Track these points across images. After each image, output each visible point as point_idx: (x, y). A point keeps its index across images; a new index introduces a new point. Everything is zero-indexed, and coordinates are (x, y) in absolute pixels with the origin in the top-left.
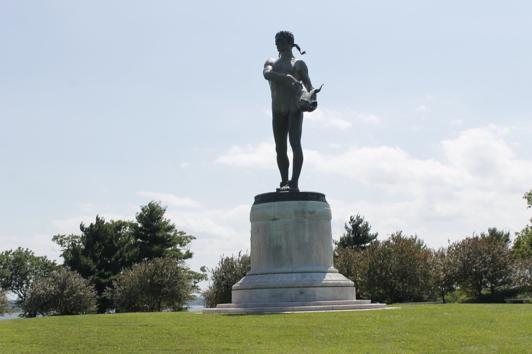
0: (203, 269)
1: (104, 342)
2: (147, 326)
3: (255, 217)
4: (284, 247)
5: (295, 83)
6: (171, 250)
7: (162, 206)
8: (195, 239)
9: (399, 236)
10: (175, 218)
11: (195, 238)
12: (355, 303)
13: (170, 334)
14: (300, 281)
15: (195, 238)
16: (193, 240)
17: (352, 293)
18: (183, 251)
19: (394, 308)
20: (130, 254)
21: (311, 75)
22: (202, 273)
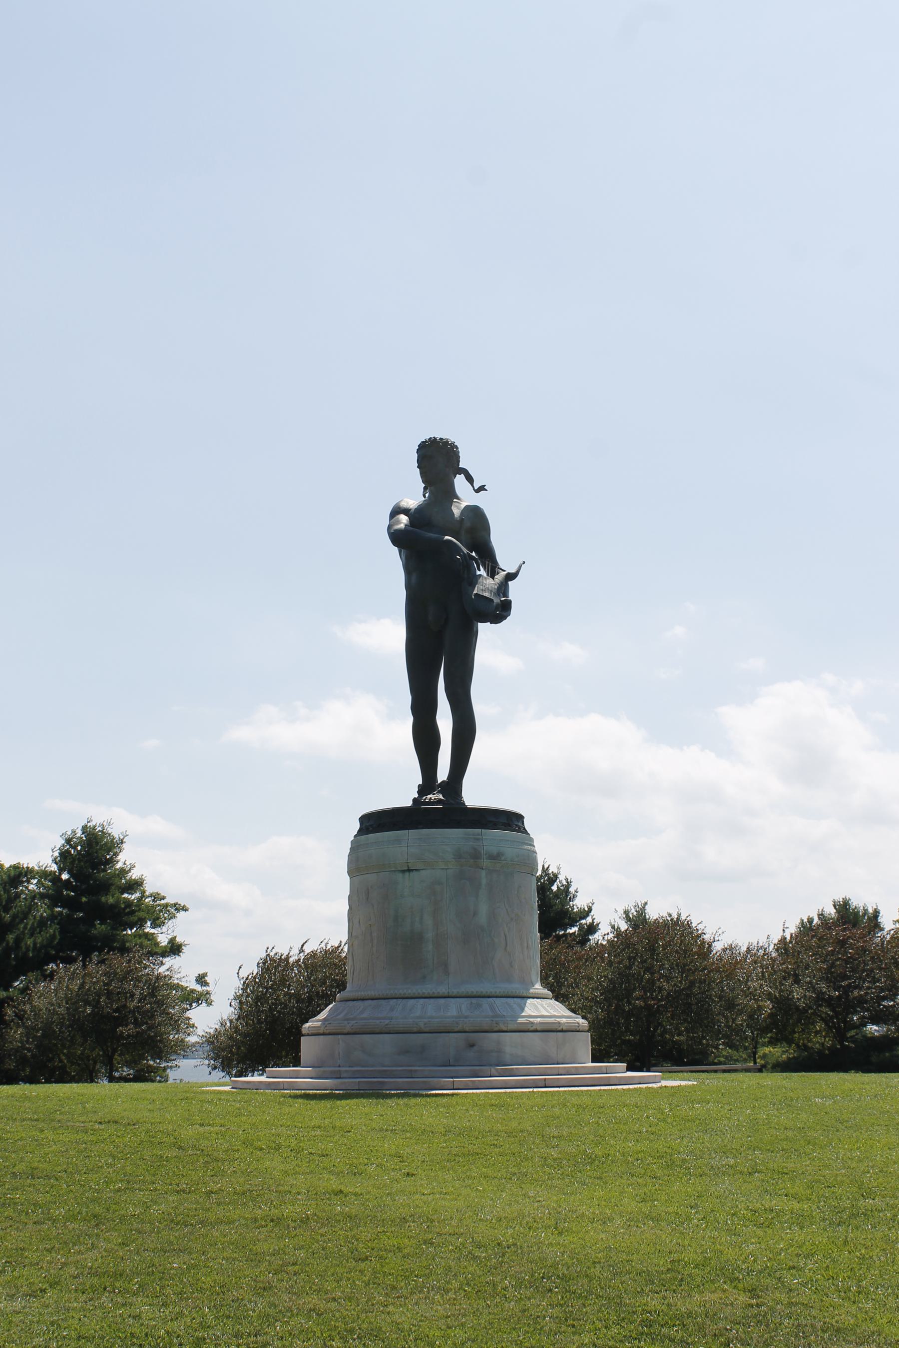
0: (201, 979)
1: (21, 1167)
2: (116, 1122)
3: (359, 864)
4: (430, 935)
5: (464, 556)
6: (134, 935)
7: (115, 832)
8: (186, 910)
9: (641, 912)
10: (149, 861)
11: (185, 909)
12: (628, 1081)
13: (180, 1148)
14: (466, 1017)
15: (185, 909)
16: (182, 913)
17: (584, 1045)
18: (163, 940)
19: (683, 1083)
20: (39, 940)
21: (498, 540)
22: (198, 988)
